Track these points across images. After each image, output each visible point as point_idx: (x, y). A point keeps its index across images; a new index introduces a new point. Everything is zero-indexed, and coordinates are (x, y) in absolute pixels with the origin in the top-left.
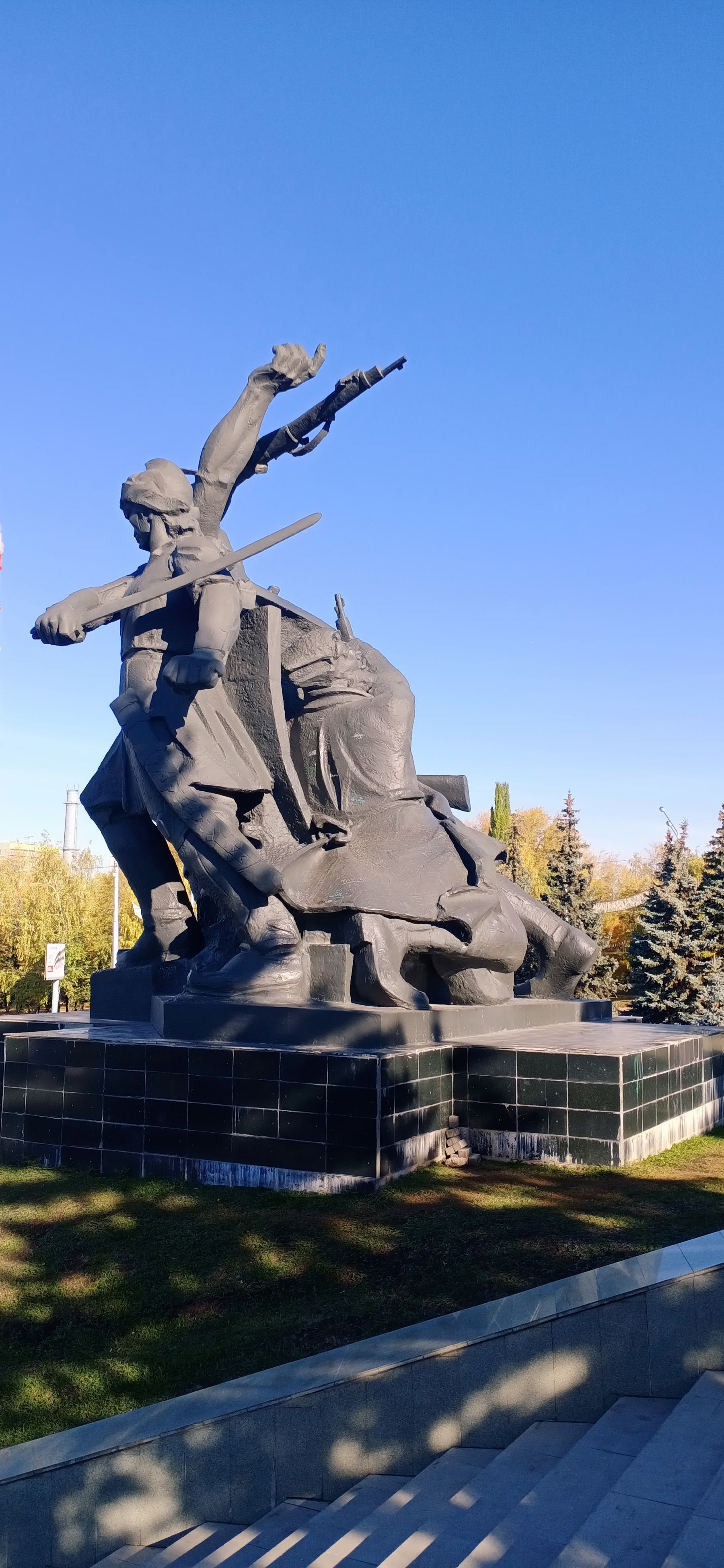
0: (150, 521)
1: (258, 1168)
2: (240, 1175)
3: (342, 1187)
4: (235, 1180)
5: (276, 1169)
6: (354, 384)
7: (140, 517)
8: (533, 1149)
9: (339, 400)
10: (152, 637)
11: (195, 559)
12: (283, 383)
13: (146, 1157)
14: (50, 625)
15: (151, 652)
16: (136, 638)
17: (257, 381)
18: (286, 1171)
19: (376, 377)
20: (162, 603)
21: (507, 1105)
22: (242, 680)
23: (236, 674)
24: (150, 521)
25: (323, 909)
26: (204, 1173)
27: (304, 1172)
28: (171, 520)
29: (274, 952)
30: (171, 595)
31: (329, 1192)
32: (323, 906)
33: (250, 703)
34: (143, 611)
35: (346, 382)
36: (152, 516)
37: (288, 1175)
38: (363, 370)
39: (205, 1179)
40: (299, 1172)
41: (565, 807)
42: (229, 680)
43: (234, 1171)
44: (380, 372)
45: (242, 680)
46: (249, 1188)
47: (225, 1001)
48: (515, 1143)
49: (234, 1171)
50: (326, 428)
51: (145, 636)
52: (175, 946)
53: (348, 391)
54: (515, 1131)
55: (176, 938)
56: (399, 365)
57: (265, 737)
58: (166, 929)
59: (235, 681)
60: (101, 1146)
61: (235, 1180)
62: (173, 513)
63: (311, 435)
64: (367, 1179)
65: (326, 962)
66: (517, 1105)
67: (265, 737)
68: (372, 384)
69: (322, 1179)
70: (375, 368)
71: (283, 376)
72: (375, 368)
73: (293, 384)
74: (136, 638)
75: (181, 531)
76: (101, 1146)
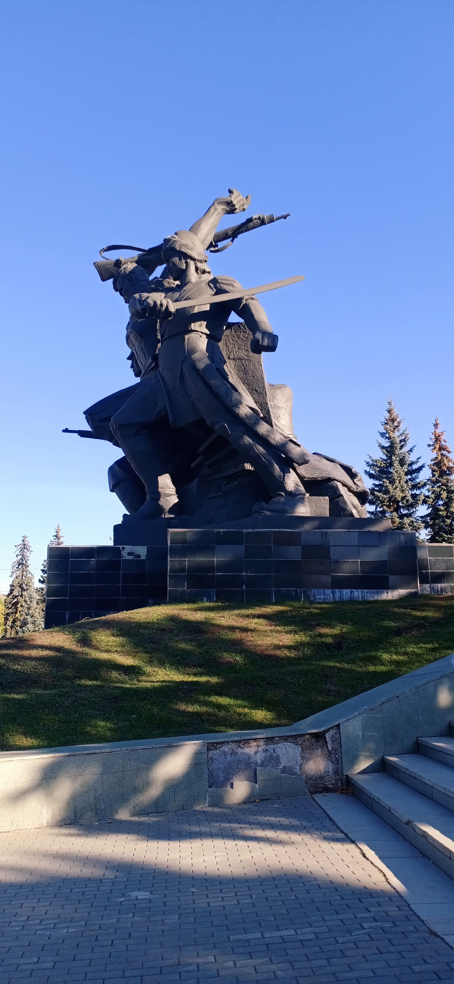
0: (187, 263)
1: (348, 591)
2: (337, 595)
3: (399, 595)
4: (334, 598)
5: (359, 590)
6: (259, 221)
7: (180, 259)
8: (438, 591)
9: (247, 227)
10: (201, 325)
11: (233, 286)
12: (232, 209)
13: (275, 591)
14: (161, 305)
15: (200, 333)
16: (192, 324)
17: (220, 204)
18: (366, 591)
19: (272, 220)
20: (207, 308)
21: (424, 572)
22: (240, 359)
23: (234, 356)
24: (187, 263)
25: (315, 478)
26: (314, 595)
27: (376, 590)
28: (199, 265)
29: (299, 497)
30: (212, 305)
31: (392, 599)
32: (314, 476)
33: (245, 372)
34: (196, 311)
35: (255, 219)
36: (189, 260)
37: (367, 592)
38: (266, 215)
39: (316, 599)
40: (373, 590)
41: (56, 534)
42: (229, 358)
43: (333, 593)
44: (275, 218)
45: (240, 359)
46: (344, 601)
47: (293, 515)
48: (429, 589)
49: (333, 593)
50: (232, 241)
51: (198, 324)
52: (171, 511)
53: (254, 223)
54: (428, 583)
55: (173, 505)
56: (285, 217)
57: (256, 391)
58: (166, 500)
59: (234, 359)
60: (244, 587)
61: (334, 598)
62: (201, 261)
63: (221, 245)
64: (413, 591)
65: (316, 506)
66: (430, 571)
67: (256, 391)
68: (268, 223)
69: (387, 593)
70: (272, 215)
71: (234, 205)
72: (272, 215)
73: (235, 212)
74: (192, 324)
75: (204, 272)
76: (244, 587)
